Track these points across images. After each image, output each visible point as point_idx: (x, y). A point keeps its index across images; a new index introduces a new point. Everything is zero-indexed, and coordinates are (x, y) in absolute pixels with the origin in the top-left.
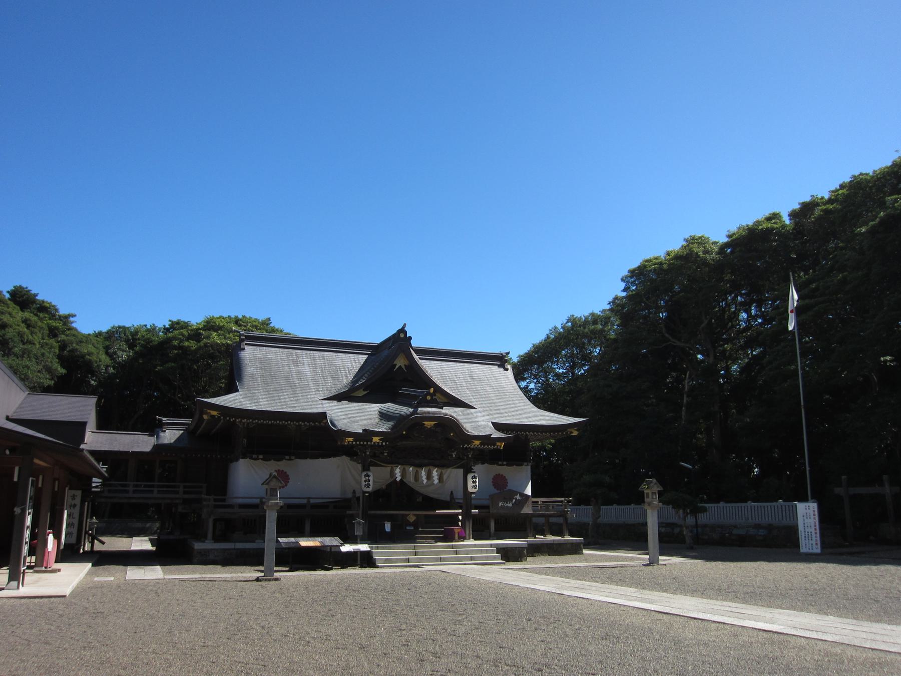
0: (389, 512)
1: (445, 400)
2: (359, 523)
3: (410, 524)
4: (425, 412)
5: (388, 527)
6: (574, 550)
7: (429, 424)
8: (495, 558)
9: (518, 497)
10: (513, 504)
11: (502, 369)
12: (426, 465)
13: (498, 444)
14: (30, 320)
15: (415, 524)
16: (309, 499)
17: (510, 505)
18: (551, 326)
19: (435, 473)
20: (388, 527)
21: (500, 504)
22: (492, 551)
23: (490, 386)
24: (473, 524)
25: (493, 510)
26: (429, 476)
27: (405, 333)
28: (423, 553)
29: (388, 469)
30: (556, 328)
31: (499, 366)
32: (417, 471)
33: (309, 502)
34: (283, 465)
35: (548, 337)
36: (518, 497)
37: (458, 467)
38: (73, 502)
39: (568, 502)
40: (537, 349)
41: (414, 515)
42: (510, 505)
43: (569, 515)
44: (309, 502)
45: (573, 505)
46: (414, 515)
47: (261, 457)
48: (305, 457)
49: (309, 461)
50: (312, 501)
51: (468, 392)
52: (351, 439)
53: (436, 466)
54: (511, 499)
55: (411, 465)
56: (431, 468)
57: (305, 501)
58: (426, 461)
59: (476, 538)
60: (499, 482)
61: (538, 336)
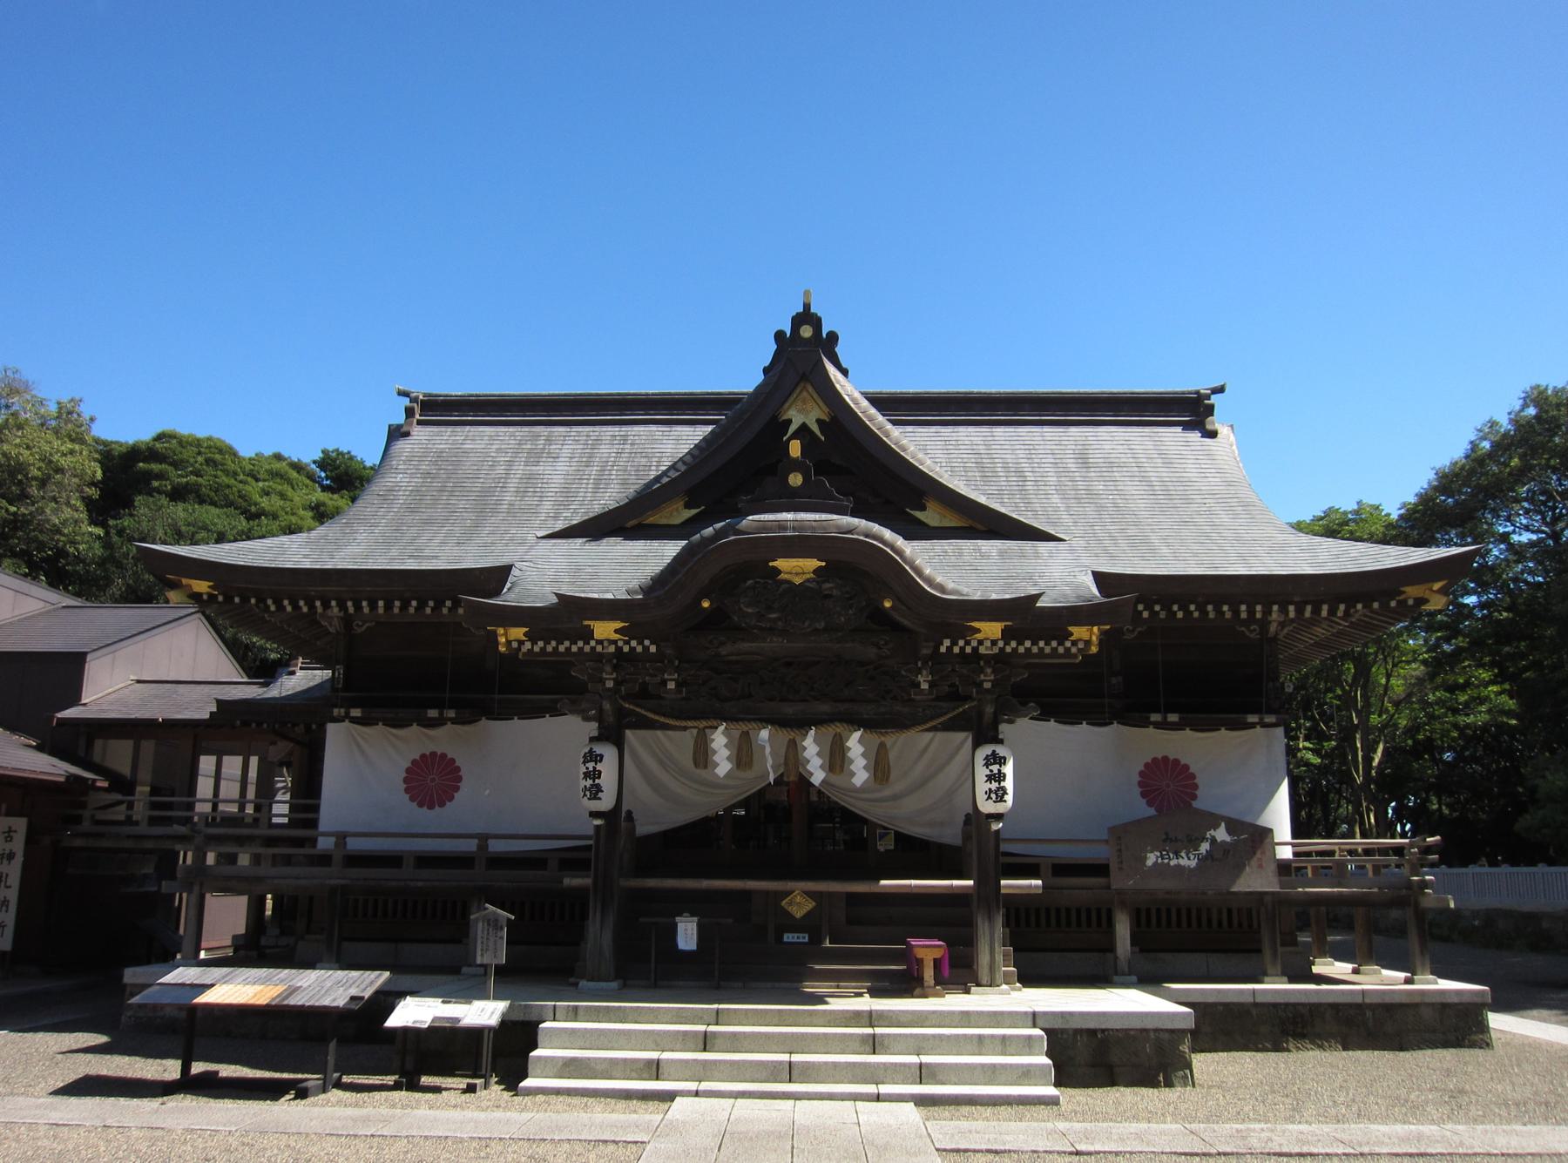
0: (706, 884)
1: (951, 521)
2: (494, 923)
3: (796, 926)
4: (764, 527)
5: (687, 934)
6: (1458, 1028)
7: (797, 568)
8: (1026, 1074)
9: (1221, 834)
10: (1203, 860)
11: (1195, 436)
12: (818, 721)
13: (1079, 632)
14: (324, 504)
15: (810, 924)
16: (483, 838)
17: (1188, 861)
18: (1480, 420)
19: (855, 744)
20: (687, 934)
21: (1152, 858)
22: (1027, 1044)
23: (1144, 479)
24: (1007, 924)
25: (1118, 881)
26: (836, 759)
27: (816, 322)
28: (735, 1043)
29: (678, 742)
30: (1493, 424)
31: (1187, 426)
32: (746, 734)
33: (483, 847)
34: (445, 739)
35: (1474, 446)
36: (1221, 834)
37: (949, 727)
38: (8, 847)
39: (1428, 850)
40: (1448, 481)
41: (810, 894)
42: (1188, 861)
43: (1430, 898)
44: (483, 847)
45: (1442, 861)
46: (810, 894)
47: (356, 713)
48: (503, 714)
49: (517, 723)
50: (496, 846)
51: (1056, 499)
52: (518, 633)
53: (856, 722)
54: (1192, 842)
55: (766, 721)
56: (839, 728)
57: (471, 846)
58: (825, 708)
59: (1029, 979)
60: (1168, 787)
61: (1449, 446)
